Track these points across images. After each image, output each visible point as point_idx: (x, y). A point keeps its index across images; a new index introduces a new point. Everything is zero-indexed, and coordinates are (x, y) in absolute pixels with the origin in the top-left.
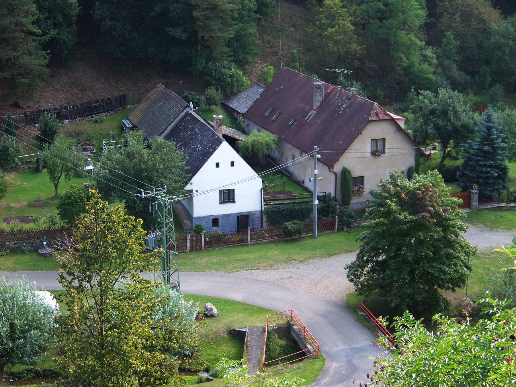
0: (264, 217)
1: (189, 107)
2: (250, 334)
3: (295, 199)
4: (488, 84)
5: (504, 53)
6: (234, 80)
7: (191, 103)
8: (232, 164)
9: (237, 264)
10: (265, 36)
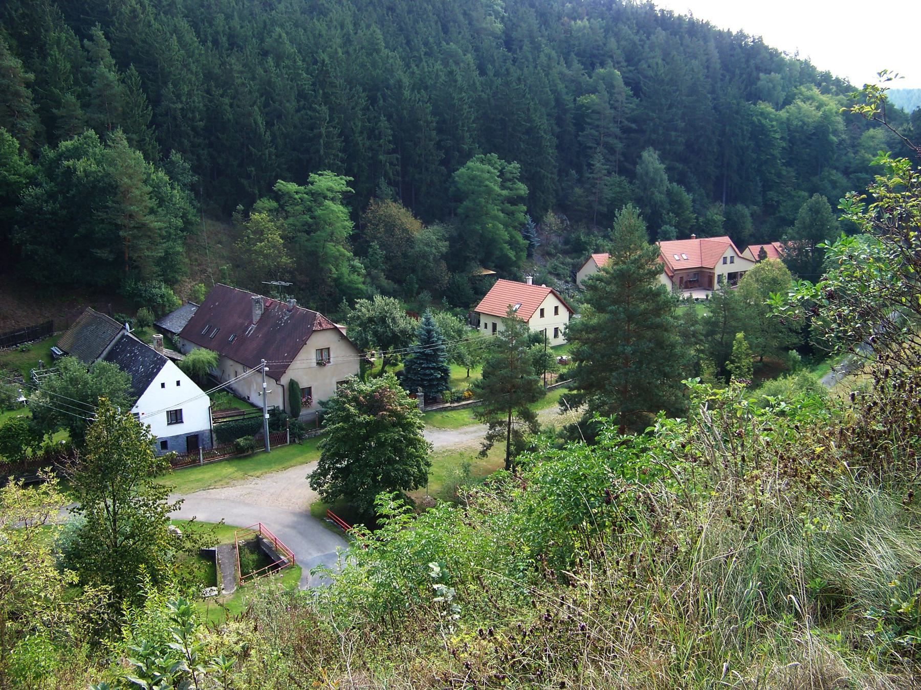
0: (214, 435)
1: (125, 328)
2: (219, 551)
3: (244, 415)
4: (415, 290)
5: (428, 260)
6: (165, 300)
7: (127, 325)
8: (178, 383)
9: (192, 485)
10: (192, 254)
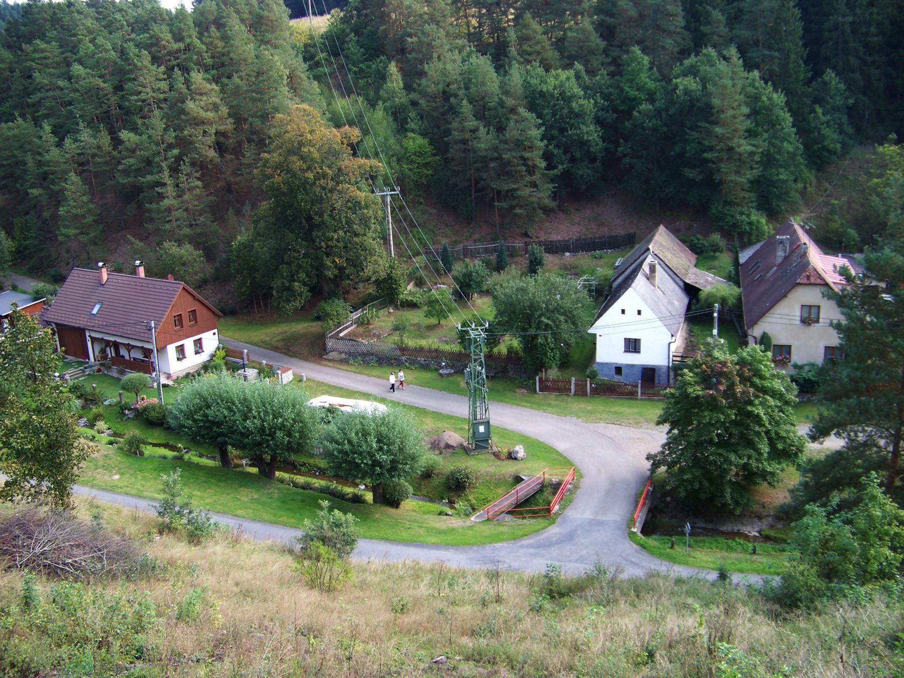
8: (639, 312)
